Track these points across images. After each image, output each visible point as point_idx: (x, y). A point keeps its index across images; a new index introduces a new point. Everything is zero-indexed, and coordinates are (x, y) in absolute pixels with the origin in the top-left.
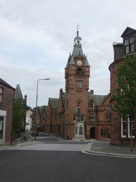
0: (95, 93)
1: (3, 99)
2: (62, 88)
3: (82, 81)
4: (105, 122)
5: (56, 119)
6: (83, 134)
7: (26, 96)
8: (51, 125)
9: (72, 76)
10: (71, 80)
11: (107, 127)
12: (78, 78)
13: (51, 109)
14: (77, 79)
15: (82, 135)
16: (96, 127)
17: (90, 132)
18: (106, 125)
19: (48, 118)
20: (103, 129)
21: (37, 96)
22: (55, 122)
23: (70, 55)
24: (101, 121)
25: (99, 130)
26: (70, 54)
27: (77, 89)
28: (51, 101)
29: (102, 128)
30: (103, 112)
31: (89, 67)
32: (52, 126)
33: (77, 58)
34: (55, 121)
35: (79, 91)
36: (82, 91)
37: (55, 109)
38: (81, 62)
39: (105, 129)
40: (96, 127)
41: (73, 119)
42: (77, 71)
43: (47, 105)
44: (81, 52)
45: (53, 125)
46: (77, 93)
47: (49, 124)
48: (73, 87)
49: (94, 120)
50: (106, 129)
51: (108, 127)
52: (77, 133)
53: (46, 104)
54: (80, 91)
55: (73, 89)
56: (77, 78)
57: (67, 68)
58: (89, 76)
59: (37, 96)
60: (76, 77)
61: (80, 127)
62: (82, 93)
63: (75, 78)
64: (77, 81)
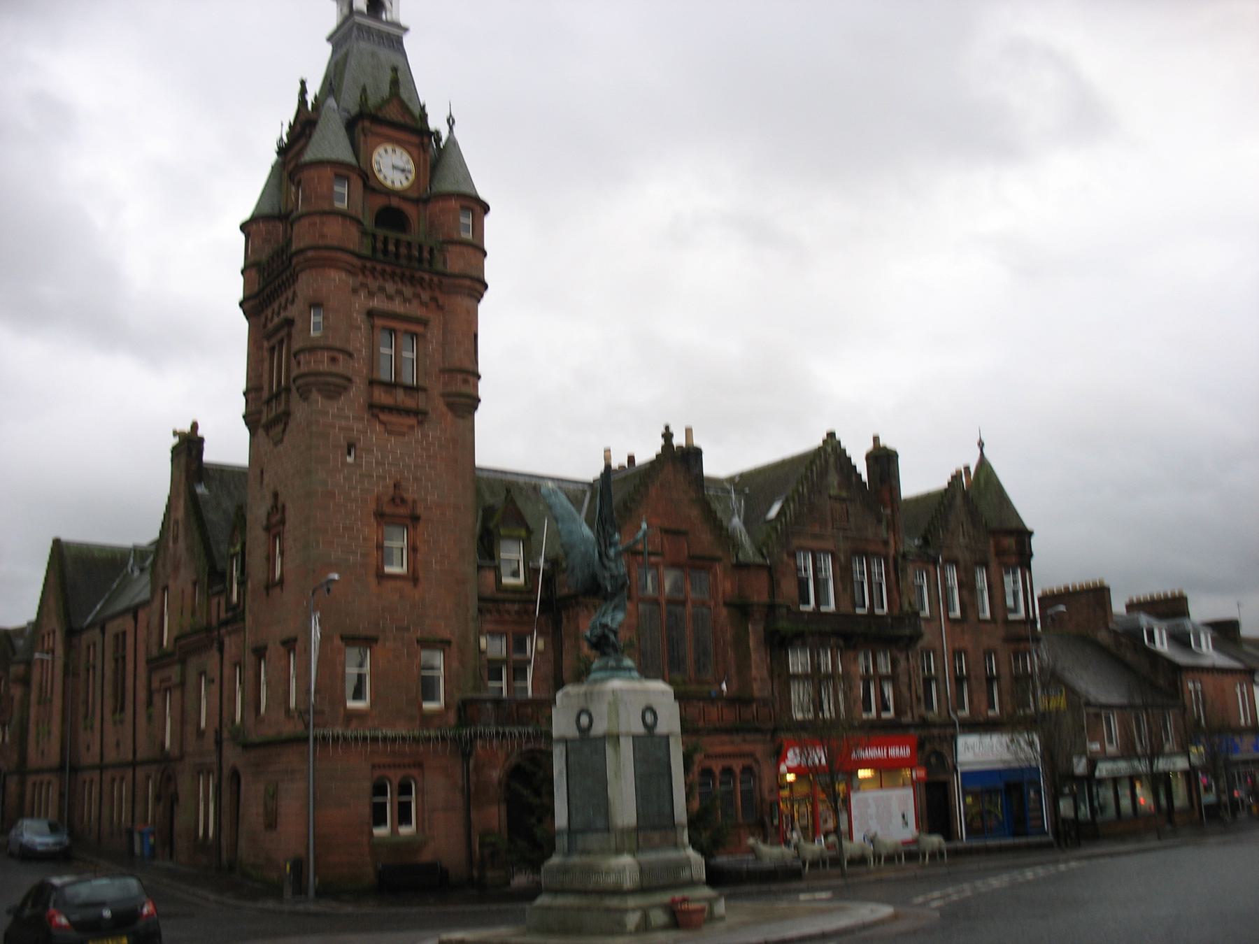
1: (570, 792)
3: (418, 329)
5: (120, 707)
8: (69, 767)
9: (332, 264)
10: (316, 305)
12: (382, 289)
14: (377, 303)
19: (44, 701)
22: (110, 739)
26: (303, 91)
27: (381, 396)
32: (75, 770)
33: (376, 119)
35: (391, 409)
36: (419, 415)
37: (113, 627)
39: (727, 762)
42: (368, 222)
44: (400, 79)
45: (90, 757)
46: (374, 435)
47: (54, 758)
48: (340, 368)
50: (737, 766)
51: (747, 748)
54: (408, 412)
55: (335, 388)
56: (371, 295)
58: (478, 287)
60: (364, 285)
62: (418, 433)
63: (355, 291)
64: (379, 322)
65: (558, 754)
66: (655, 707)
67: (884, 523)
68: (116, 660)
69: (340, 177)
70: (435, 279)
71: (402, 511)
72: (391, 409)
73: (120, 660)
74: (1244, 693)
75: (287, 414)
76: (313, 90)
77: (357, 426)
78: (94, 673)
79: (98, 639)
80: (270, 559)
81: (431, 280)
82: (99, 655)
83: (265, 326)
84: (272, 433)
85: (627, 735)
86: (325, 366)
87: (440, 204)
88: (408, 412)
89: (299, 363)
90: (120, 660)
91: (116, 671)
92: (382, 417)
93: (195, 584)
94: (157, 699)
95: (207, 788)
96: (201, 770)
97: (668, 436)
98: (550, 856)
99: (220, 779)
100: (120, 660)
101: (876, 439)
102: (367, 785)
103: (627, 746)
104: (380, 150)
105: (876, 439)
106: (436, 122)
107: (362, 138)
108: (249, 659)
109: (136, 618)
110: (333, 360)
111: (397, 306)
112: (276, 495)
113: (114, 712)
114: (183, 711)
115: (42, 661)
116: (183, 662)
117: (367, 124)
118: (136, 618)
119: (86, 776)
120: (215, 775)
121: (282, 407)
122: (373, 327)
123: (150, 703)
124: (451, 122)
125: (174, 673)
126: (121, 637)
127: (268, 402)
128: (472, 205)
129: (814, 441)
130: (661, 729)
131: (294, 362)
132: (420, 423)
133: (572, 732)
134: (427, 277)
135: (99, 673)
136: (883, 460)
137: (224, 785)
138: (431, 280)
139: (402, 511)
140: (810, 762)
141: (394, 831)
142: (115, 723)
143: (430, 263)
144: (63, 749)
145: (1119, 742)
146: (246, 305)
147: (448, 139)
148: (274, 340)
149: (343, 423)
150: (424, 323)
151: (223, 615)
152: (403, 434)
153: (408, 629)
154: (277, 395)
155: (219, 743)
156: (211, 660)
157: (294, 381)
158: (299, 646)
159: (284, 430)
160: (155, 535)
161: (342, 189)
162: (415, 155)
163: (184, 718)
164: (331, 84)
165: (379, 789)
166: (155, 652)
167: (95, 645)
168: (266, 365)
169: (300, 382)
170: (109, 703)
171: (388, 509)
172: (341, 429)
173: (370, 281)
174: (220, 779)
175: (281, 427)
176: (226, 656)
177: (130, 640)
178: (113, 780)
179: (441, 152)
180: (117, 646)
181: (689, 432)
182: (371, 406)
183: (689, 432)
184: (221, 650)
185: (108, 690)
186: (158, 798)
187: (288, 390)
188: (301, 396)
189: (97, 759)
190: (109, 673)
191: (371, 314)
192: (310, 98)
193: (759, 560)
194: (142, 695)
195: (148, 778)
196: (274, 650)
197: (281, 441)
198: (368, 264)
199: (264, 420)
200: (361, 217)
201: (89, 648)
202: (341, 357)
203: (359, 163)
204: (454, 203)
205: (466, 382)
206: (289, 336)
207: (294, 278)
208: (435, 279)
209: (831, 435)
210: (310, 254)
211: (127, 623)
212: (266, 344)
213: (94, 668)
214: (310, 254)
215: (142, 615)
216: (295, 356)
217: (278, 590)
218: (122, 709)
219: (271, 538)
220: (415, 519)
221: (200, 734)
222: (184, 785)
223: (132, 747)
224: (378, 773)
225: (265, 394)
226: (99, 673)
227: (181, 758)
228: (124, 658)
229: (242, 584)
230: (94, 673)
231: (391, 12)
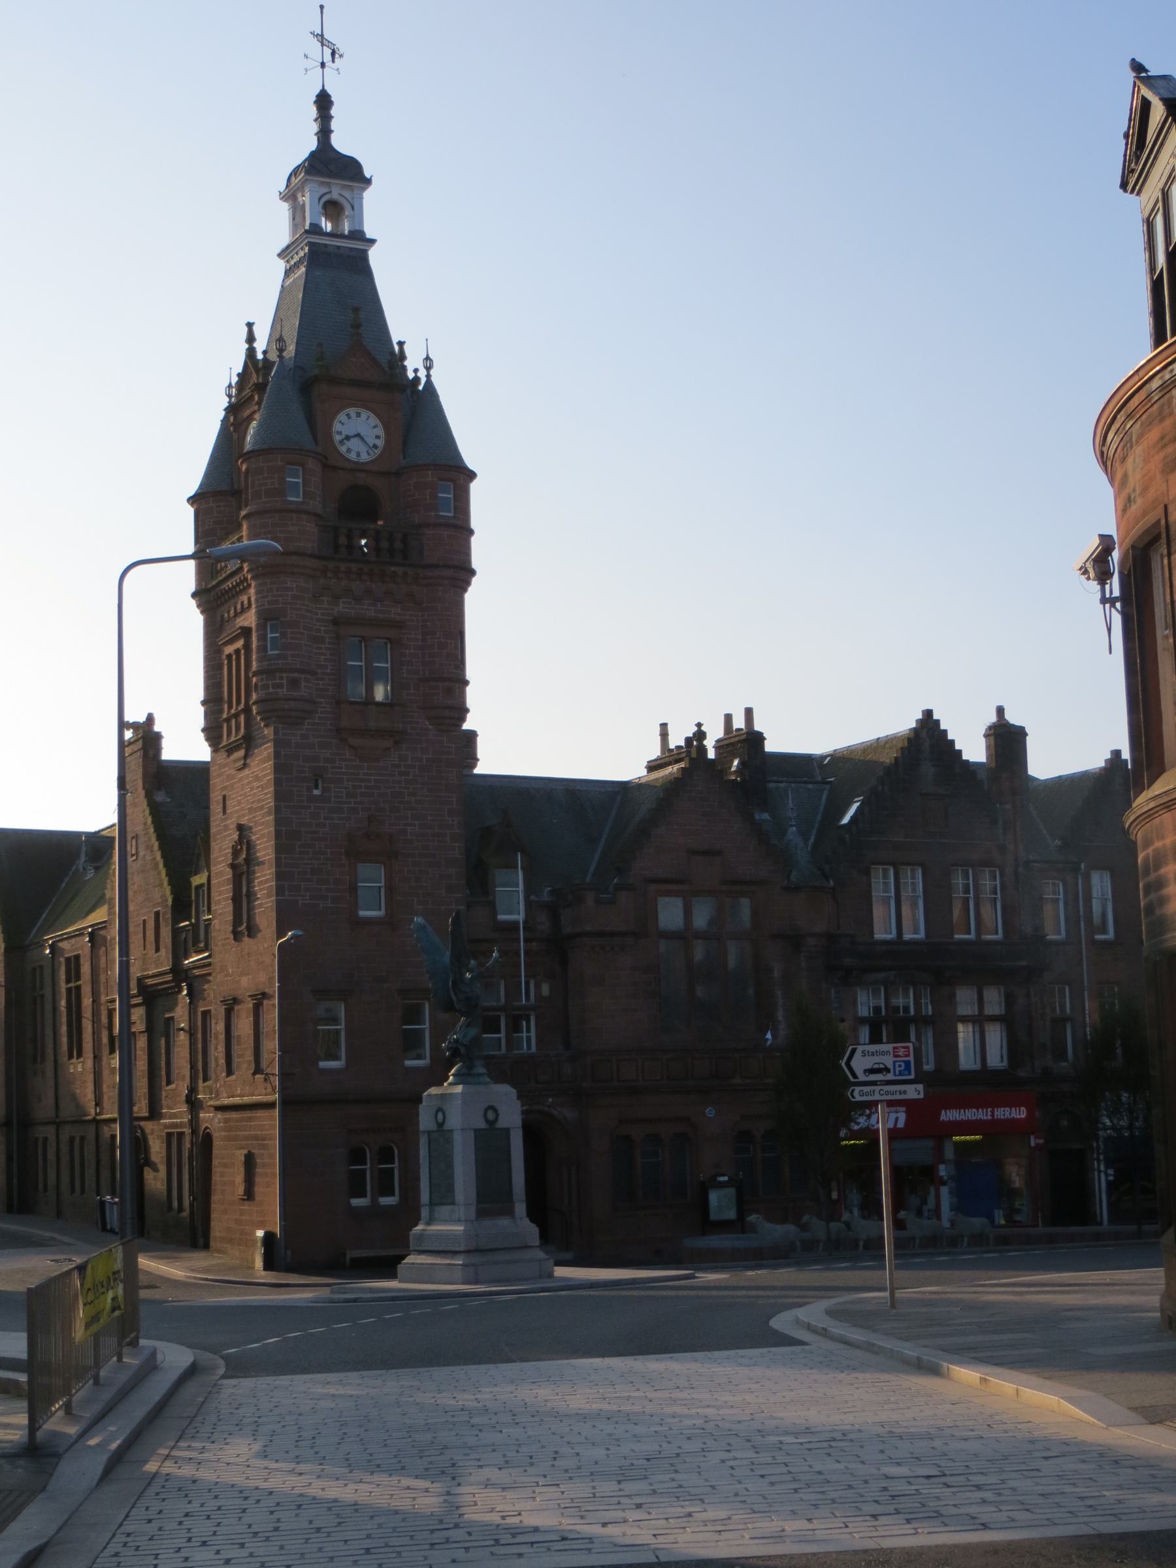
0: (770, 746)
2: (150, 719)
6: (520, 1208)
7: (401, 344)
14: (342, 608)
15: (504, 1222)
16: (568, 1114)
21: (322, 13)
23: (251, 352)
26: (251, 339)
38: (374, 420)
43: (984, 760)
49: (529, 1038)
52: (443, 1194)
53: (682, 744)
57: (221, 493)
59: (322, 13)
61: (482, 1125)
65: (423, 1142)
66: (495, 1105)
74: (193, 1184)
81: (406, 573)
85: (424, 1132)
97: (728, 718)
98: (416, 1225)
101: (1000, 711)
105: (1000, 711)
110: (294, 683)
129: (904, 722)
130: (502, 1123)
133: (432, 1126)
138: (406, 573)
140: (985, 1110)
141: (374, 1200)
160: (145, 720)
165: (357, 1156)
175: (242, 753)
179: (272, 710)
181: (749, 713)
183: (749, 713)
192: (260, 346)
209: (928, 714)
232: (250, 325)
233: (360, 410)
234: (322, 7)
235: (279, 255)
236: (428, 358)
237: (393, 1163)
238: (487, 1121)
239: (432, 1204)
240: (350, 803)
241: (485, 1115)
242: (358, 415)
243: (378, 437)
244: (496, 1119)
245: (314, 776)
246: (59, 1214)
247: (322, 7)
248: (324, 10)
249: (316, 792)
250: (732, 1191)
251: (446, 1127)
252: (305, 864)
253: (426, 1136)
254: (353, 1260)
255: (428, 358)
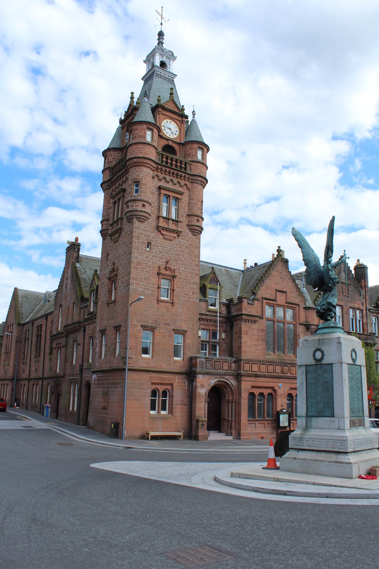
4: (261, 362)
5: (38, 355)
7: (183, 106)
11: (269, 383)
13: (19, 324)
14: (163, 184)
17: (207, 404)
18: (264, 376)
20: (257, 392)
22: (33, 368)
24: (248, 361)
25: (243, 395)
27: (162, 223)
28: (20, 299)
29: (253, 387)
30: (255, 326)
31: (204, 147)
34: (33, 363)
35: (167, 230)
38: (175, 125)
40: (232, 382)
41: (140, 350)
42: (160, 149)
46: (157, 239)
50: (266, 392)
54: (173, 231)
58: (204, 181)
64: (163, 192)
67: (362, 296)
68: (37, 336)
69: (149, 129)
70: (187, 176)
71: (168, 273)
72: (167, 230)
73: (39, 336)
75: (121, 229)
76: (136, 96)
77: (152, 235)
78: (28, 342)
79: (31, 328)
80: (110, 292)
82: (30, 333)
83: (112, 194)
84: (113, 238)
85: (300, 366)
86: (140, 208)
87: (189, 146)
88: (173, 231)
89: (128, 207)
90: (39, 336)
91: (37, 341)
92: (163, 232)
93: (74, 303)
94: (54, 352)
95: (74, 391)
96: (72, 382)
99: (81, 386)
100: (39, 336)
102: (149, 391)
103: (345, 367)
104: (165, 121)
106: (188, 112)
107: (158, 115)
108: (98, 335)
109: (47, 319)
111: (170, 186)
112: (114, 264)
113: (36, 357)
114: (66, 357)
115: (8, 335)
116: (67, 336)
117: (160, 110)
118: (47, 319)
119: (23, 383)
120: (79, 384)
121: (119, 226)
122: (160, 194)
123: (51, 353)
124: (194, 113)
125: (63, 341)
126: (40, 327)
127: (112, 225)
128: (203, 147)
131: (125, 206)
132: (178, 236)
134: (183, 175)
135: (30, 342)
136: (361, 270)
137: (83, 388)
138: (185, 176)
139: (168, 273)
142: (35, 361)
143: (185, 169)
144: (14, 371)
145: (227, 408)
146: (104, 186)
147: (193, 120)
148: (116, 199)
149: (146, 233)
150: (181, 194)
151: (86, 317)
152: (171, 240)
153: (169, 325)
154: (117, 221)
155: (81, 370)
156: (80, 336)
157: (125, 214)
158: (122, 328)
159: (119, 236)
161: (149, 133)
162: (179, 125)
163: (66, 360)
164: (145, 94)
165: (154, 393)
166: (54, 333)
167: (29, 330)
168: (112, 210)
169: (128, 214)
170: (34, 353)
171: (163, 271)
172: (145, 236)
173: (159, 174)
174: (81, 386)
176: (86, 334)
177: (44, 328)
178: (34, 384)
180: (38, 330)
182: (158, 227)
184: (84, 331)
185: (34, 348)
186: (52, 393)
187: (122, 219)
188: (128, 221)
189: (27, 376)
190: (34, 341)
191: (160, 188)
192: (135, 100)
193: (314, 306)
194: (48, 350)
195: (48, 384)
196: (110, 331)
197: (117, 241)
198: (160, 167)
199: (110, 232)
200: (157, 147)
201: (26, 331)
202: (146, 204)
203: (156, 123)
204: (195, 146)
205: (198, 220)
206: (123, 196)
207: (127, 172)
208: (187, 176)
210: (135, 160)
211: (43, 322)
212: (112, 201)
213: (28, 339)
214: (135, 160)
215: (49, 318)
216: (126, 204)
217: (113, 305)
218: (39, 356)
219: (111, 282)
220: (174, 277)
221: (73, 367)
222: (64, 388)
223: (42, 371)
224: (154, 387)
225: (111, 222)
226: (30, 342)
227: (64, 377)
228: (41, 335)
229: (96, 303)
230: (28, 342)
231: (169, 68)
232: (132, 93)
233: (171, 121)
234: (162, 7)
235: (142, 79)
236: (194, 112)
237: (166, 398)
238: (315, 359)
239: (308, 416)
240: (160, 255)
241: (314, 355)
242: (171, 122)
243: (177, 131)
244: (322, 359)
245: (148, 242)
246: (27, 409)
247: (162, 7)
248: (163, 8)
249: (148, 249)
250: (287, 415)
251: (324, 361)
252: (142, 275)
253: (303, 369)
254: (152, 436)
255: (194, 112)
